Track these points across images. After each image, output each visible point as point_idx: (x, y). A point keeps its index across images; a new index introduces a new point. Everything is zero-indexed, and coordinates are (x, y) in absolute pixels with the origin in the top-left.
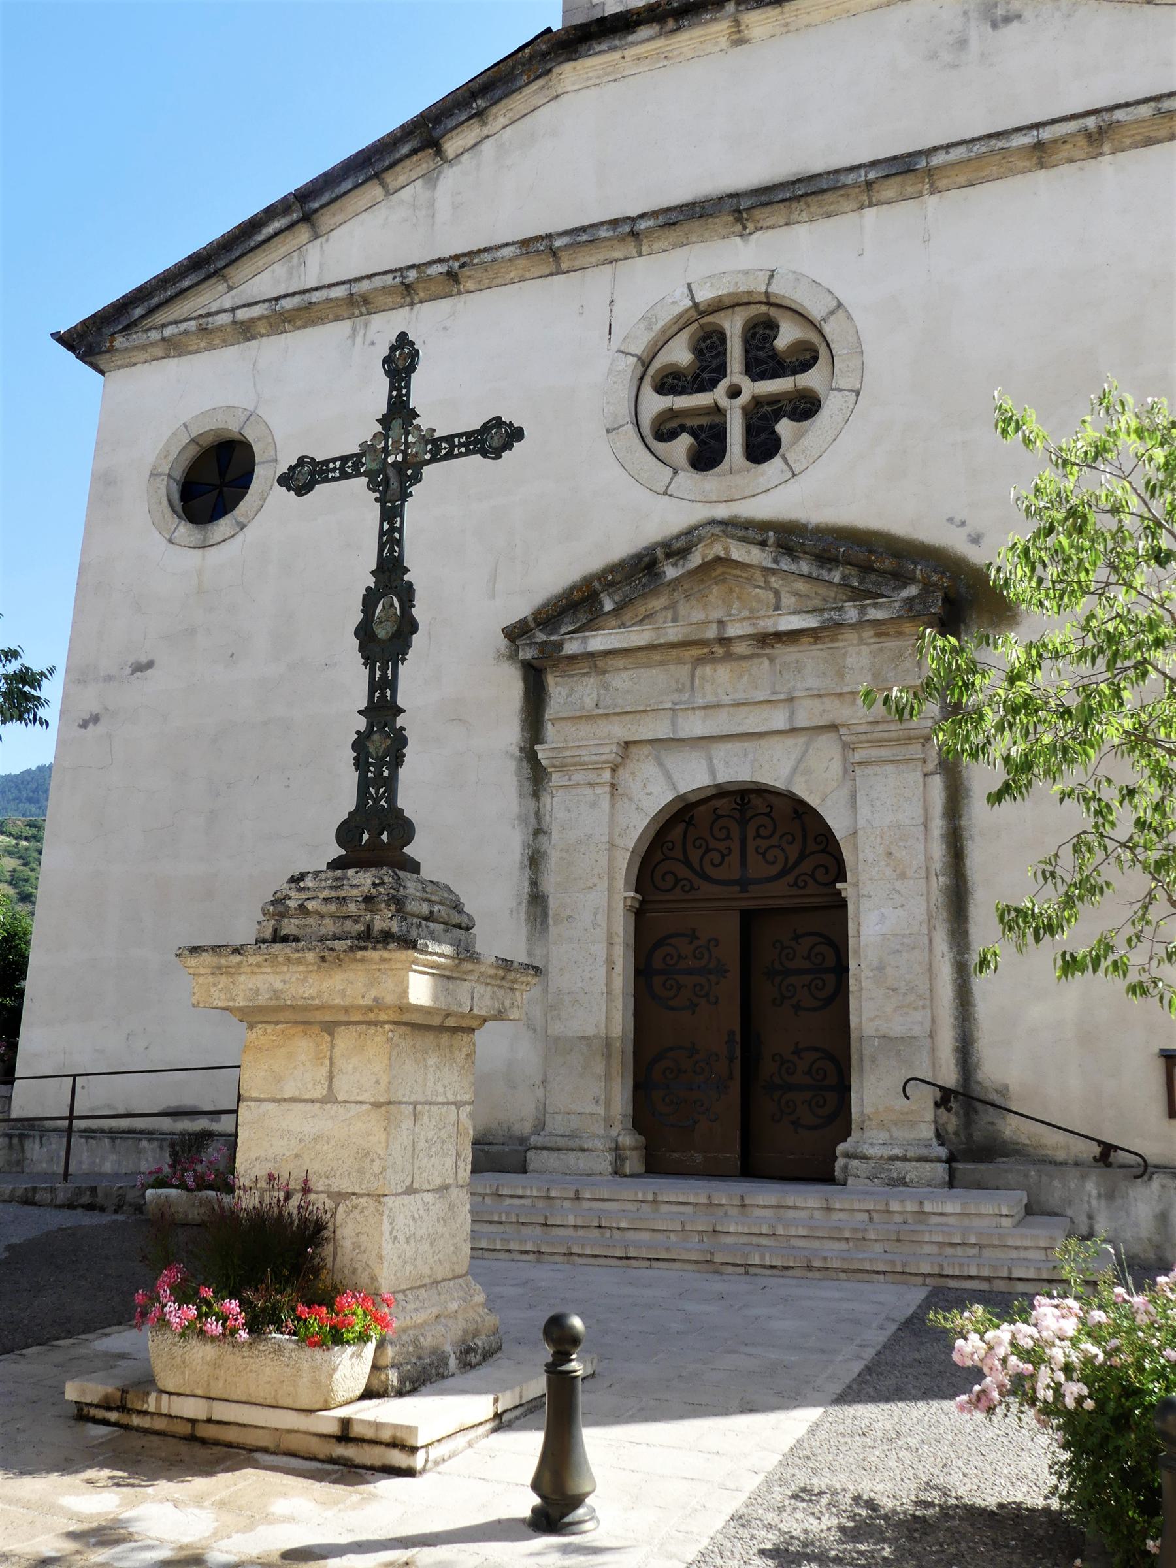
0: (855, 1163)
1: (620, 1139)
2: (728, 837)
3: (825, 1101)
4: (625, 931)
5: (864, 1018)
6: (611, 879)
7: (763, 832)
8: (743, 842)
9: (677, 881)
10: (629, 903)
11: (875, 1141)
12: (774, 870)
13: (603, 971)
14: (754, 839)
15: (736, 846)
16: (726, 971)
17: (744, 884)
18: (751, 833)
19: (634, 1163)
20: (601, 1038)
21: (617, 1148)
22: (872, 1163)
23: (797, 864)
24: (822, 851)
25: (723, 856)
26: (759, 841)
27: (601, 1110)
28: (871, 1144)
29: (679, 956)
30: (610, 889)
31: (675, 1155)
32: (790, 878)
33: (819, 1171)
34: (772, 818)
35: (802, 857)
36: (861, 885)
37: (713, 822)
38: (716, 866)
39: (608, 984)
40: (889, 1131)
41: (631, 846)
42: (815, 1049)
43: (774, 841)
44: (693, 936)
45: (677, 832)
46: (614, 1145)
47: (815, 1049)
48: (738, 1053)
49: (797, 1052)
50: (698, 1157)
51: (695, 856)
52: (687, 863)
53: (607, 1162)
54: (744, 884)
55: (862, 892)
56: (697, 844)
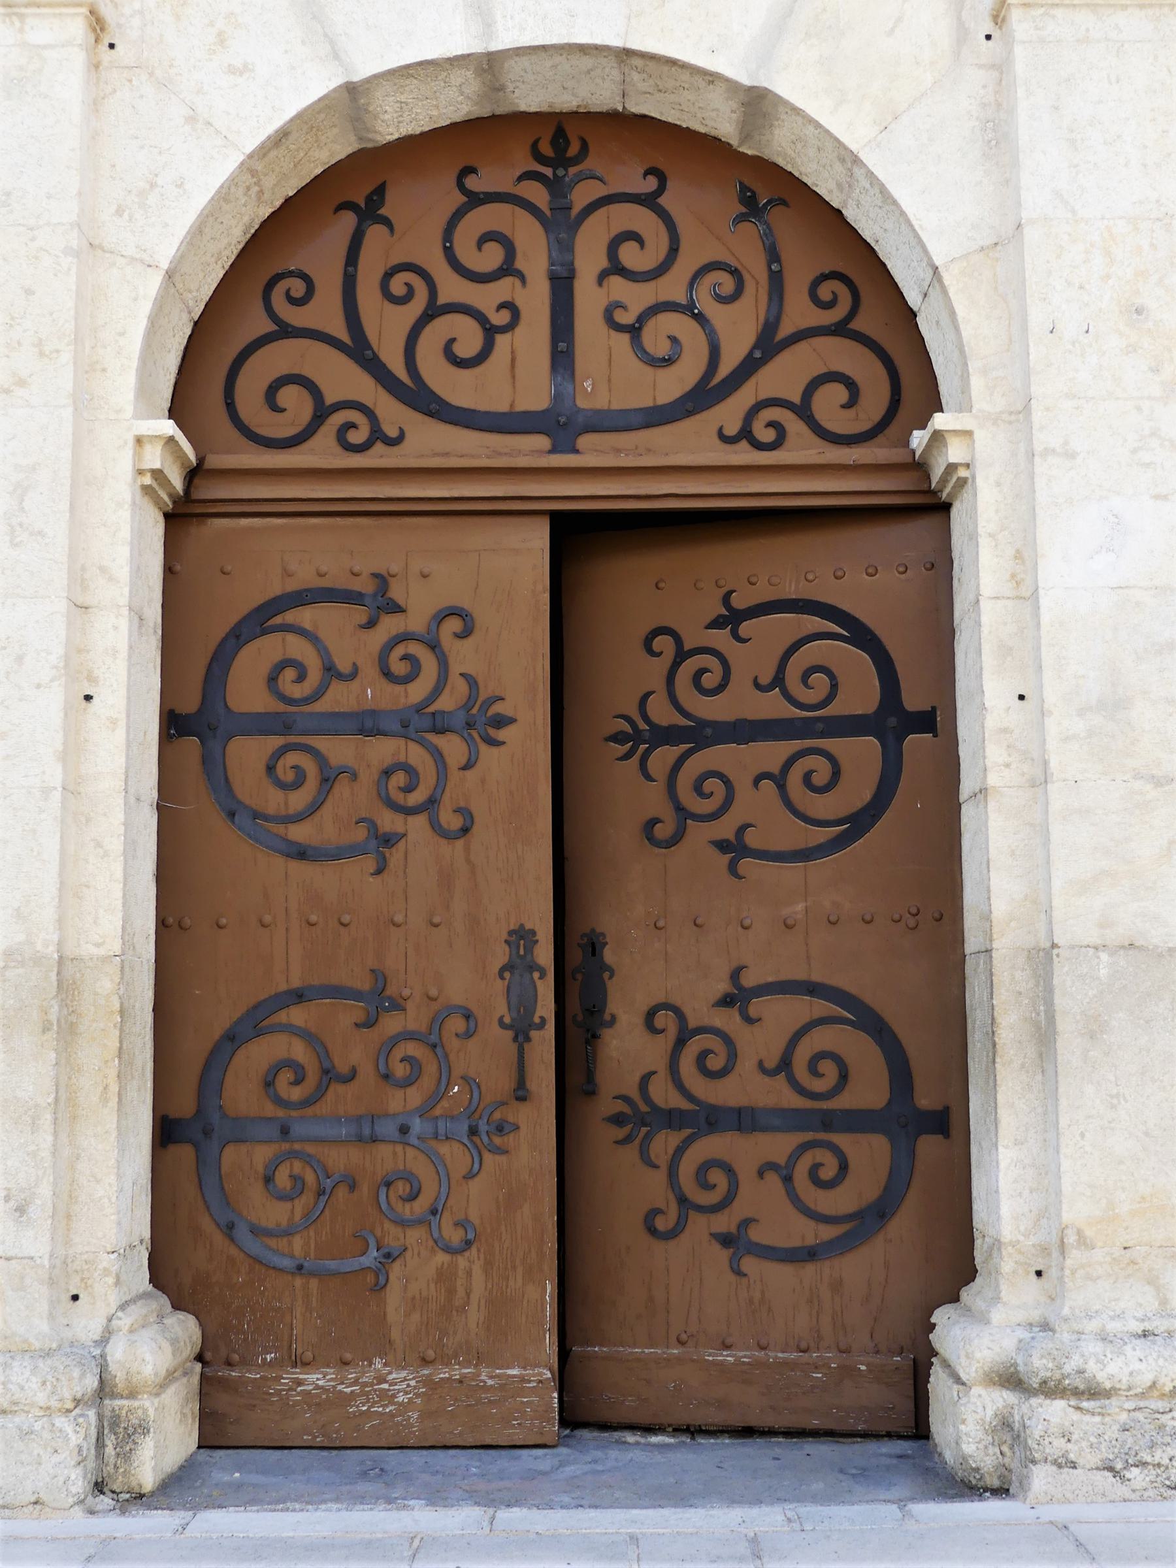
0: (1056, 1411)
1: (117, 1352)
2: (508, 269)
3: (844, 1167)
4: (137, 571)
5: (1057, 884)
6: (88, 369)
7: (629, 255)
8: (562, 285)
9: (321, 413)
10: (154, 458)
11: (1113, 1326)
12: (671, 385)
13: (52, 703)
14: (602, 277)
15: (535, 300)
16: (501, 722)
17: (561, 425)
18: (589, 256)
19: (167, 1436)
20: (38, 960)
21: (104, 1389)
22: (1119, 1411)
23: (748, 367)
24: (840, 329)
25: (490, 332)
26: (618, 287)
27: (36, 1243)
28: (1104, 1337)
29: (330, 671)
30: (84, 402)
31: (315, 1379)
32: (729, 413)
33: (879, 1417)
34: (664, 216)
35: (768, 345)
36: (1038, 416)
37: (458, 215)
38: (461, 363)
39: (73, 750)
40: (1152, 1281)
41: (166, 253)
42: (812, 989)
43: (672, 287)
44: (380, 601)
45: (322, 252)
46: (92, 1382)
47: (812, 989)
48: (546, 1006)
49: (736, 998)
50: (402, 1382)
51: (387, 328)
52: (360, 350)
53: (67, 1456)
54: (561, 425)
55: (1041, 440)
56: (397, 286)
